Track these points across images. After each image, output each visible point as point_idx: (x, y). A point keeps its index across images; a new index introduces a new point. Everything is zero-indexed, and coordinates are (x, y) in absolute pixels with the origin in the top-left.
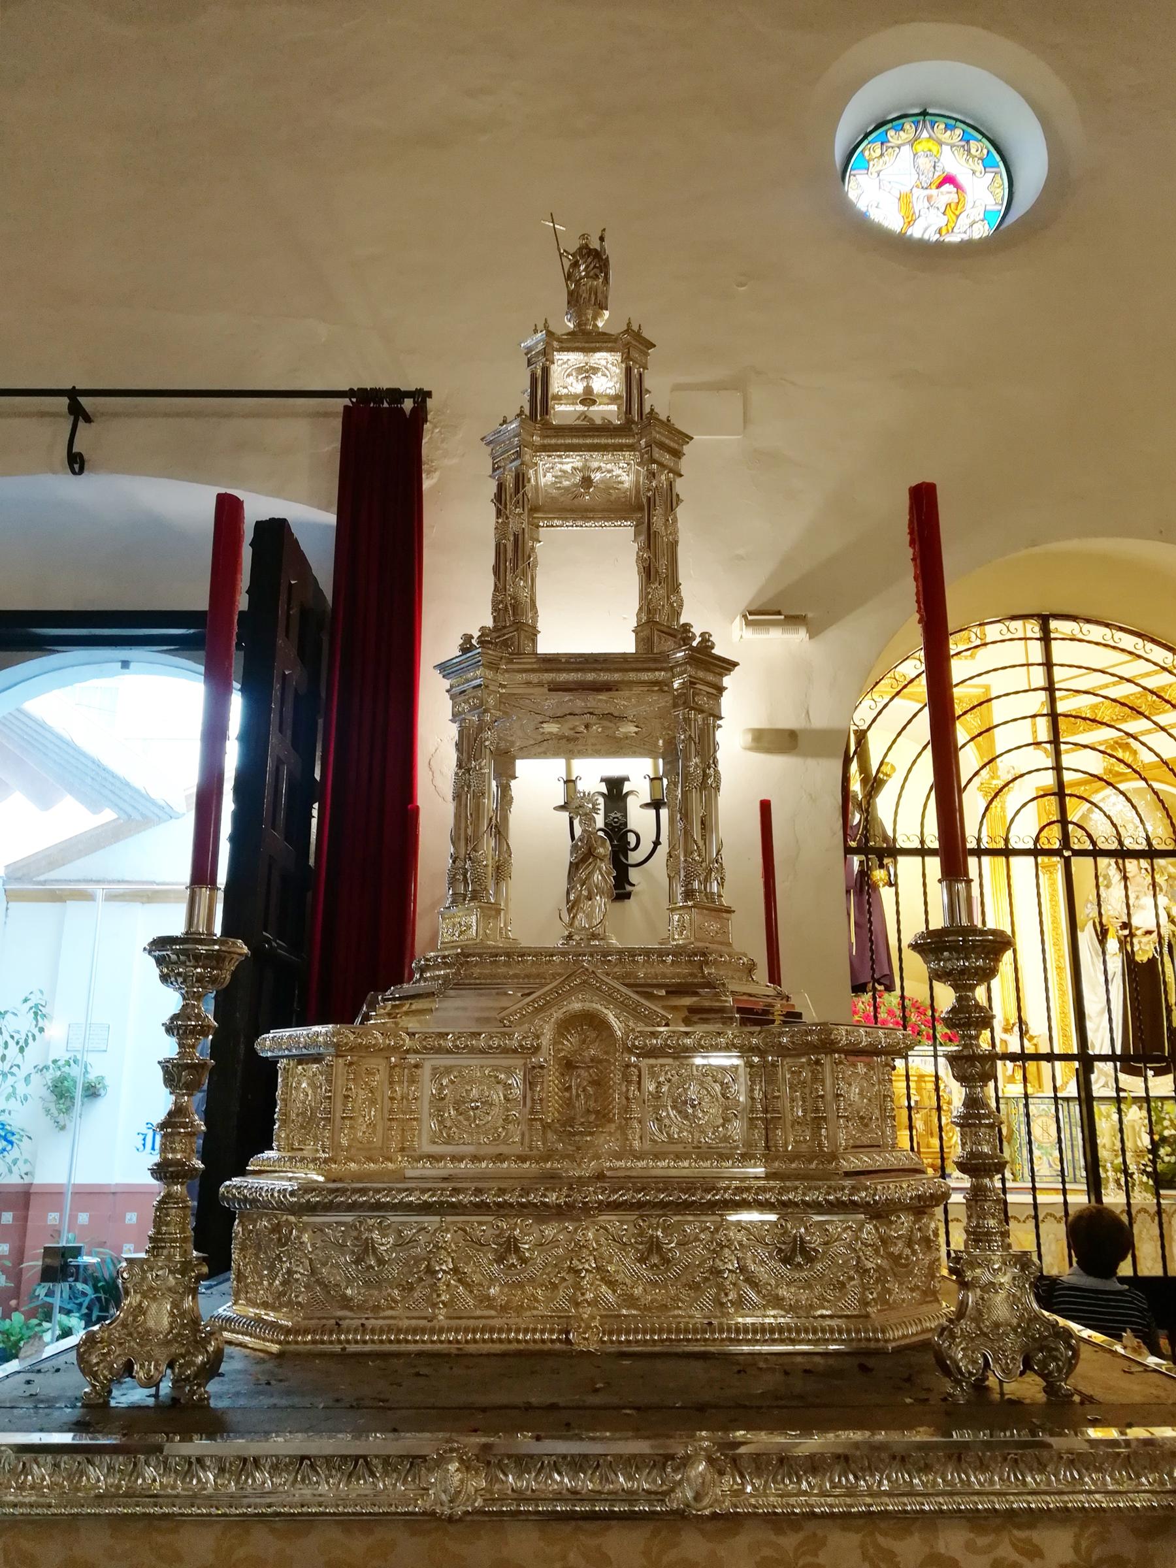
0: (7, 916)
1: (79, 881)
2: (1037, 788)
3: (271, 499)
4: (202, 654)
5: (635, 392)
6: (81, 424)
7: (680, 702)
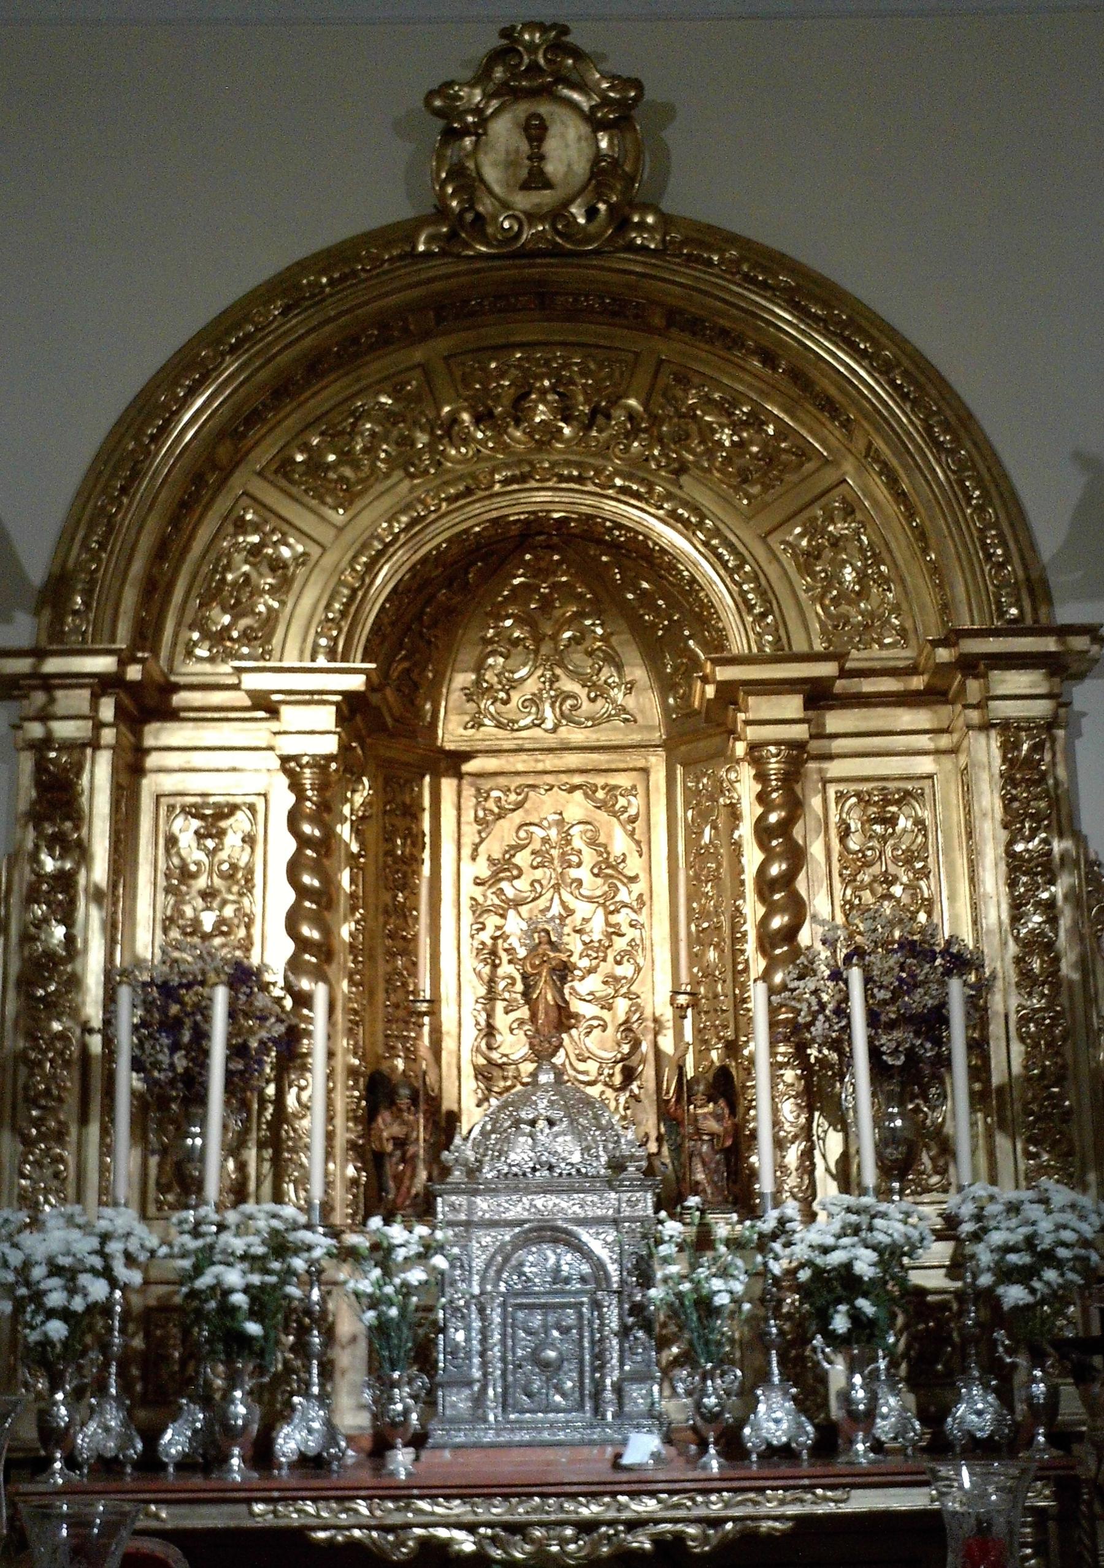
1: (522, 1486)
2: (667, 112)
3: (170, 353)
4: (278, 1425)
6: (943, 1271)
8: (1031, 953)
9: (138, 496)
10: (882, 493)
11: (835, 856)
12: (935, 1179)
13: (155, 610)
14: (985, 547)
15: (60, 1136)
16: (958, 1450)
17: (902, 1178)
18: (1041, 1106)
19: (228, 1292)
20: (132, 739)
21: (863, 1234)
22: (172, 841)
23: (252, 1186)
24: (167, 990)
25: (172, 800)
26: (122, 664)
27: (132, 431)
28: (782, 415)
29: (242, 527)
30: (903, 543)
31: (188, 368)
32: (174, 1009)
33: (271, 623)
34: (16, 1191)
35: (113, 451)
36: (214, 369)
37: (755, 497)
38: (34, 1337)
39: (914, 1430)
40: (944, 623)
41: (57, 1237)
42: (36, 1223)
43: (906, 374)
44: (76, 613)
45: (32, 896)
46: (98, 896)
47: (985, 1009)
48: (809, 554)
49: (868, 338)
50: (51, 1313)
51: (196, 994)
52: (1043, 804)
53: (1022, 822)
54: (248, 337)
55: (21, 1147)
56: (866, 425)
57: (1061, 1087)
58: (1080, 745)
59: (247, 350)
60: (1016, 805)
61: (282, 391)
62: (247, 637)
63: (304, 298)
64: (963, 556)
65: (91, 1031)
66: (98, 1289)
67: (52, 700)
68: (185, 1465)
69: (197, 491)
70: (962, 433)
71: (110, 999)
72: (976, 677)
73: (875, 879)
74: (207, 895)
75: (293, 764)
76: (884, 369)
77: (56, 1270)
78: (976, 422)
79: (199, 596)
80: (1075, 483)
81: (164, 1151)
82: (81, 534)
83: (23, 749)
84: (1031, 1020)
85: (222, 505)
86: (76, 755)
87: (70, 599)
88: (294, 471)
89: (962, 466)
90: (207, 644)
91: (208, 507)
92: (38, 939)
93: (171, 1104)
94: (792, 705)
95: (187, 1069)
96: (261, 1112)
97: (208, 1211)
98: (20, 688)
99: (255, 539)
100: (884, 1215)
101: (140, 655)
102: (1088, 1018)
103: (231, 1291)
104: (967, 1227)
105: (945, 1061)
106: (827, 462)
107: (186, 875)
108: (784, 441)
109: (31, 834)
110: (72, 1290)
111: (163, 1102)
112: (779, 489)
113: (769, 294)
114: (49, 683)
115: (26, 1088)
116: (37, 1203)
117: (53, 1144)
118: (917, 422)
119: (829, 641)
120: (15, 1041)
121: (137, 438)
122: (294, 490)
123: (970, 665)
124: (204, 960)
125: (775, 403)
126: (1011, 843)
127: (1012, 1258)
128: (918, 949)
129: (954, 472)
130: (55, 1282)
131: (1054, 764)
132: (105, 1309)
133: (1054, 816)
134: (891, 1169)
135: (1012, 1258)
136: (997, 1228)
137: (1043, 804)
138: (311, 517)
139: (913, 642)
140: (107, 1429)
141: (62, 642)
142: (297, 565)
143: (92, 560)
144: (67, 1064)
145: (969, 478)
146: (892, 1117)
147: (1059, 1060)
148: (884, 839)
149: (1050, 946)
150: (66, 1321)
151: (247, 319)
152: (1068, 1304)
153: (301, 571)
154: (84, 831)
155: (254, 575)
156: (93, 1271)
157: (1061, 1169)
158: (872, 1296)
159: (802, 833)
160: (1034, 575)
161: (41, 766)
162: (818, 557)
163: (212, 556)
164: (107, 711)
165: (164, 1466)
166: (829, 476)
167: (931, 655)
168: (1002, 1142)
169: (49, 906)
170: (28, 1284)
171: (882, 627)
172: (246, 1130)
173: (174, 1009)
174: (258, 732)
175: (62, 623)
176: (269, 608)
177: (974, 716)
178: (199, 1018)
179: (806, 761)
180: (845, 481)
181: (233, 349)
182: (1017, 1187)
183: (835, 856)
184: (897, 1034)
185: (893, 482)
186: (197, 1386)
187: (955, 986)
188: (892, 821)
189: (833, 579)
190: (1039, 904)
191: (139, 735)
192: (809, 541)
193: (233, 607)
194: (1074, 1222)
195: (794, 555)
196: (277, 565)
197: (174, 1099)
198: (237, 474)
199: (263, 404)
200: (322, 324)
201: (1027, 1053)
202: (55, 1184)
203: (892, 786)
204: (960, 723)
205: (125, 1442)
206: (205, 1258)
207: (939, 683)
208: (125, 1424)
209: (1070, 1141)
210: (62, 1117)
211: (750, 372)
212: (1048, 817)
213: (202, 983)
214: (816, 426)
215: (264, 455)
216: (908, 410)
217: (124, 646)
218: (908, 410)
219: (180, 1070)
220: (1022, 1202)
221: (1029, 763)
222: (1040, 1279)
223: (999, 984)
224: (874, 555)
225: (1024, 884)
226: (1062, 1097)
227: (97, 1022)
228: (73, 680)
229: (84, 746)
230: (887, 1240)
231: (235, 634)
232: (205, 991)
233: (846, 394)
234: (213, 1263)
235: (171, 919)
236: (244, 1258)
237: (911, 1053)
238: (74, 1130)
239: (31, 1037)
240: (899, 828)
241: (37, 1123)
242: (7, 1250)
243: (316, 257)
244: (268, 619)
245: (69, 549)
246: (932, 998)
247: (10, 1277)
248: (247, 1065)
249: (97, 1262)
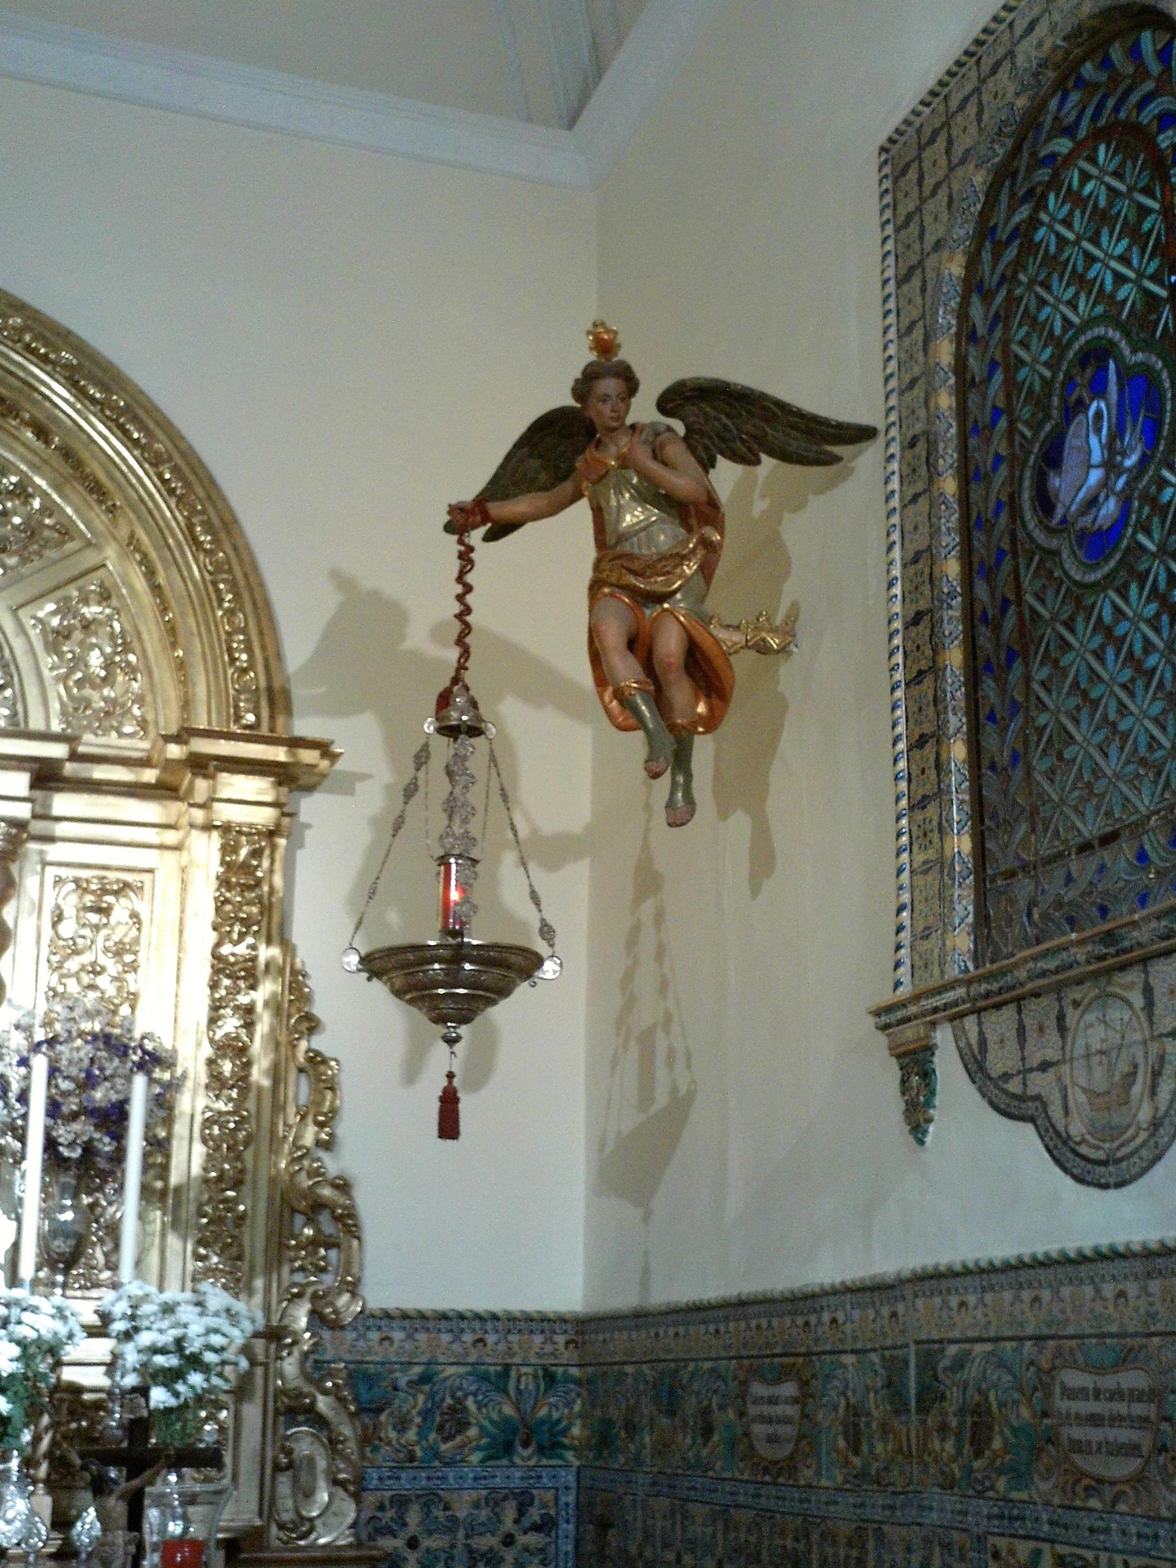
0: (492, 751)
5: (180, 560)
6: (103, 1369)
7: (1070, 84)
8: (224, 1056)
10: (140, 583)
11: (45, 941)
12: (106, 1275)
14: (230, 650)
16: (84, 1556)
17: (66, 1272)
18: (215, 1209)
21: (11, 1327)
28: (50, 491)
30: (156, 635)
37: (12, 568)
39: (39, 1535)
40: (184, 720)
43: (175, 470)
47: (171, 1109)
48: (58, 633)
49: (142, 428)
52: (255, 910)
53: (231, 926)
56: (132, 516)
57: (237, 1192)
58: (301, 856)
60: (228, 907)
64: (209, 657)
70: (223, 536)
72: (206, 776)
73: (83, 968)
76: (155, 461)
78: (240, 528)
80: (329, 601)
84: (216, 1122)
89: (218, 569)
94: (19, 782)
100: (34, 1309)
102: (273, 1124)
104: (119, 1326)
105: (119, 1157)
106: (89, 544)
108: (50, 516)
112: (37, 563)
113: (49, 368)
118: (180, 518)
119: (68, 723)
123: (200, 765)
125: (43, 477)
126: (218, 945)
127: (160, 1360)
128: (113, 1044)
129: (210, 573)
131: (271, 871)
133: (264, 923)
134: (57, 1262)
135: (160, 1360)
136: (148, 1329)
137: (255, 910)
139: (152, 733)
145: (223, 581)
146: (63, 1209)
147: (239, 1165)
148: (96, 928)
149: (243, 1050)
152: (221, 1408)
157: (230, 1273)
158: (9, 1393)
159: (13, 914)
160: (277, 684)
162: (67, 637)
166: (90, 558)
167: (162, 751)
168: (174, 1242)
171: (123, 715)
177: (199, 815)
179: (26, 840)
180: (104, 566)
182: (183, 1290)
183: (45, 941)
184: (76, 1126)
185: (150, 574)
187: (139, 1082)
188: (105, 911)
189: (79, 661)
190: (237, 1008)
192: (62, 620)
194: (226, 1327)
195: (44, 632)
201: (208, 1155)
203: (112, 875)
204: (184, 821)
207: (170, 779)
209: (241, 1245)
211: (23, 444)
212: (258, 923)
214: (84, 508)
216: (173, 505)
218: (173, 505)
220: (178, 1304)
221: (246, 868)
222: (185, 1382)
223: (189, 1084)
224: (124, 644)
225: (226, 988)
226: (236, 1201)
230: (32, 1335)
233: (112, 478)
237: (89, 1149)
240: (113, 920)
246: (117, 1092)
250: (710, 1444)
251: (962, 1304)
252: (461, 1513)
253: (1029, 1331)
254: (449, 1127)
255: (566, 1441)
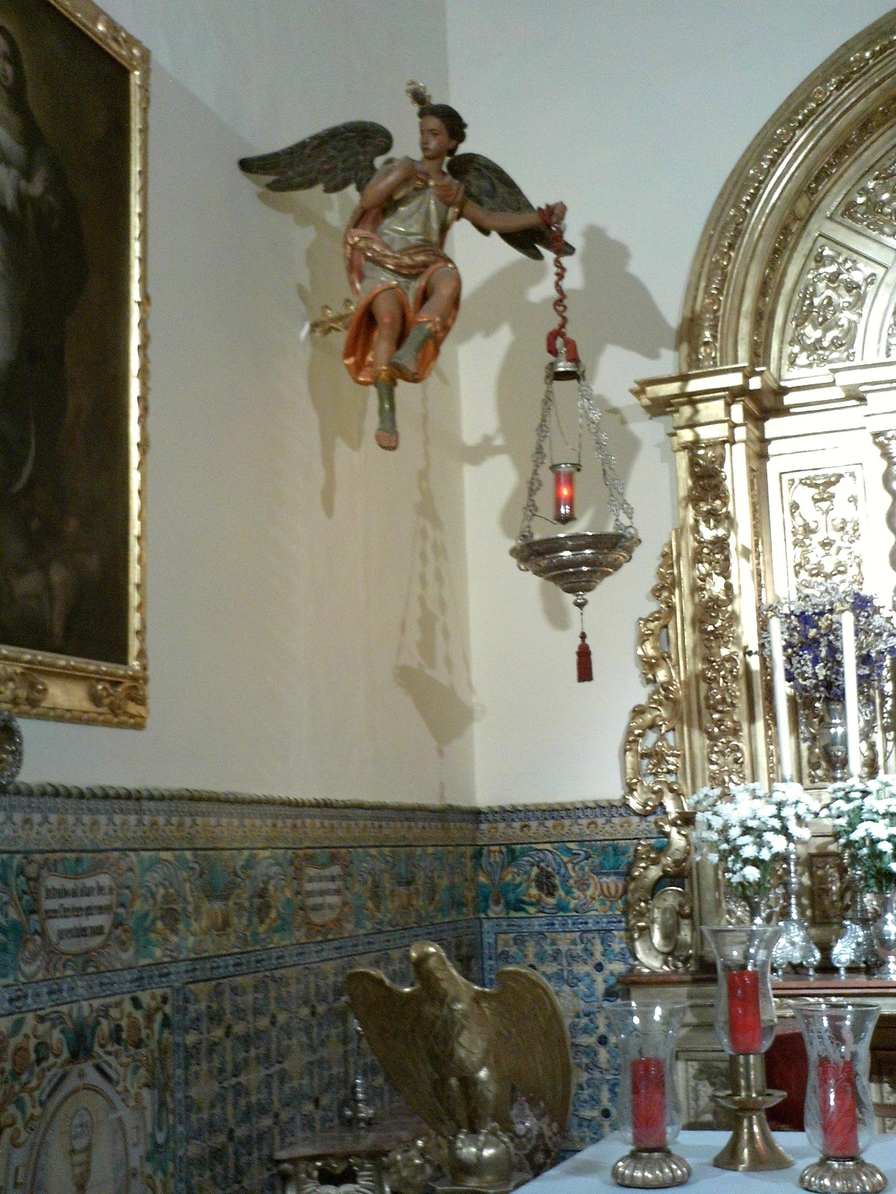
9: (742, 250)
13: (763, 335)
15: (735, 732)
19: (874, 842)
20: (757, 433)
22: (795, 506)
23: (881, 761)
24: (803, 618)
25: (791, 476)
26: (747, 378)
27: (731, 202)
29: (820, 260)
31: (770, 145)
32: (812, 632)
33: (852, 332)
34: (707, 773)
35: (719, 218)
36: (789, 142)
38: (736, 879)
41: (744, 807)
42: (726, 796)
44: (706, 344)
45: (697, 558)
46: (746, 553)
50: (746, 862)
51: (827, 619)
54: (812, 112)
55: (708, 742)
59: (813, 122)
61: (842, 150)
62: (836, 344)
63: (853, 73)
65: (750, 653)
66: (779, 844)
67: (696, 412)
68: (852, 969)
69: (785, 239)
71: (763, 627)
74: (826, 544)
75: (881, 439)
77: (747, 830)
79: (795, 318)
81: (814, 738)
82: (703, 284)
83: (678, 451)
85: (804, 246)
86: (719, 450)
87: (700, 335)
88: (856, 212)
90: (805, 354)
91: (794, 248)
92: (705, 589)
93: (818, 702)
95: (826, 676)
96: (882, 706)
97: (854, 782)
98: (671, 405)
99: (833, 269)
101: (757, 369)
103: (879, 841)
107: (808, 531)
109: (691, 512)
110: (760, 844)
111: (809, 703)
114: (692, 399)
115: (707, 698)
116: (724, 782)
117: (731, 738)
120: (695, 664)
121: (736, 206)
122: (858, 226)
124: (830, 593)
130: (748, 839)
132: (781, 858)
138: (875, 246)
140: (793, 944)
141: (698, 368)
142: (867, 284)
143: (713, 304)
144: (735, 678)
150: (757, 867)
151: (809, 99)
153: (871, 289)
154: (730, 508)
155: (835, 297)
156: (773, 829)
161: (693, 463)
163: (801, 287)
164: (737, 412)
165: (837, 970)
169: (710, 564)
170: (727, 841)
172: (874, 719)
173: (812, 632)
174: (854, 415)
175: (697, 353)
176: (850, 321)
178: (831, 637)
181: (801, 124)
186: (855, 911)
191: (762, 430)
193: (821, 324)
196: (851, 287)
197: (819, 699)
198: (813, 220)
199: (828, 163)
200: (870, 90)
202: (736, 766)
205: (808, 953)
206: (856, 817)
208: (805, 940)
210: (735, 718)
213: (831, 611)
215: (833, 202)
217: (746, 364)
219: (821, 678)
227: (754, 647)
228: (709, 395)
229: (724, 442)
231: (825, 344)
232: (835, 617)
234: (862, 821)
235: (800, 565)
236: (884, 816)
238: (745, 726)
239: (707, 660)
241: (719, 723)
242: (710, 817)
243: (858, 38)
244: (849, 329)
245: (695, 297)
247: (715, 837)
248: (872, 671)
249: (777, 824)
250: (268, 921)
251: (27, 821)
252: (564, 947)
253: (20, 846)
254: (585, 672)
255: (526, 899)
